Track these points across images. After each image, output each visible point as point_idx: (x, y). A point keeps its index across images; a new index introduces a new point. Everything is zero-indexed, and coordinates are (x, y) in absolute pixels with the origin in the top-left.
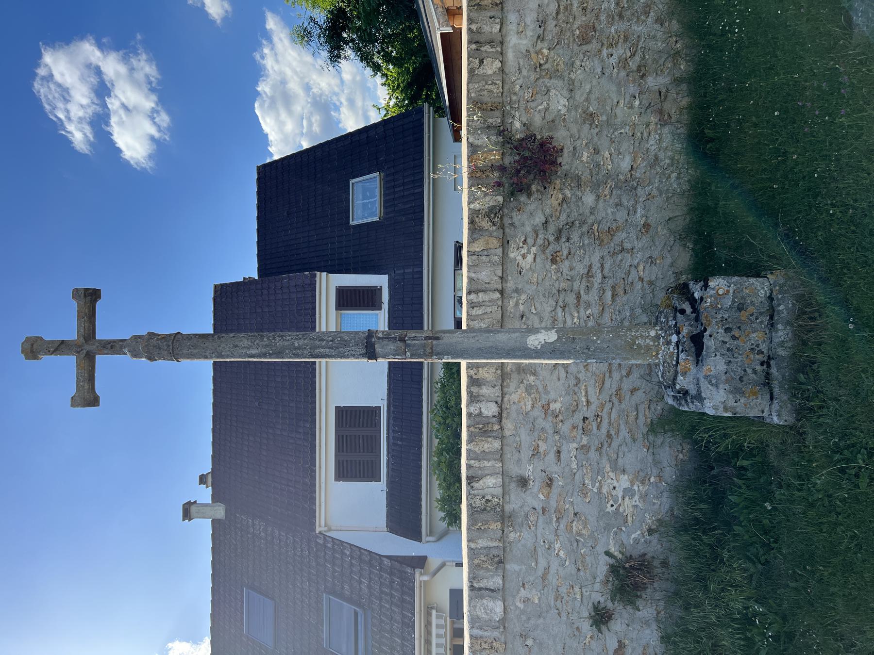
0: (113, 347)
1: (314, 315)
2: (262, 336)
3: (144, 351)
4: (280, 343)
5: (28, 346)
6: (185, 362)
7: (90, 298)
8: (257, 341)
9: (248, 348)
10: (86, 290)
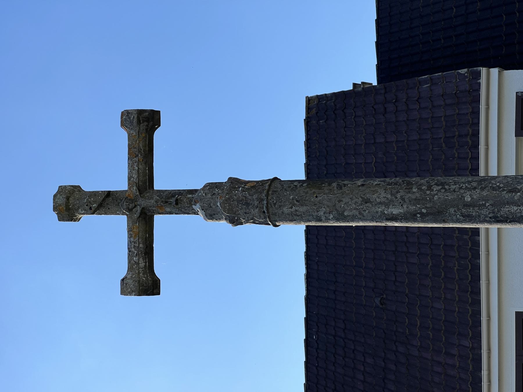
0: (179, 202)
1: (476, 146)
2: (409, 183)
3: (224, 208)
4: (439, 196)
5: (62, 200)
6: (249, 228)
7: (143, 125)
8: (402, 193)
9: (387, 205)
10: (140, 112)
